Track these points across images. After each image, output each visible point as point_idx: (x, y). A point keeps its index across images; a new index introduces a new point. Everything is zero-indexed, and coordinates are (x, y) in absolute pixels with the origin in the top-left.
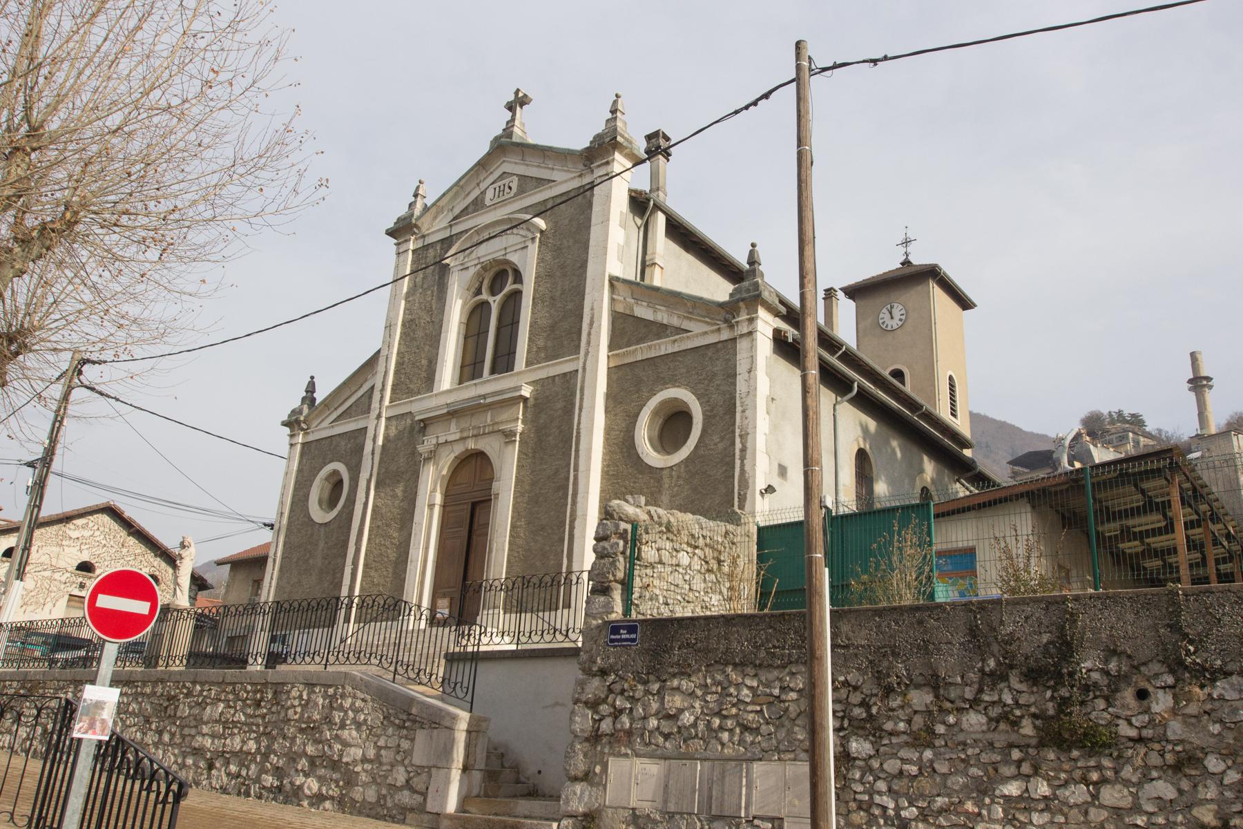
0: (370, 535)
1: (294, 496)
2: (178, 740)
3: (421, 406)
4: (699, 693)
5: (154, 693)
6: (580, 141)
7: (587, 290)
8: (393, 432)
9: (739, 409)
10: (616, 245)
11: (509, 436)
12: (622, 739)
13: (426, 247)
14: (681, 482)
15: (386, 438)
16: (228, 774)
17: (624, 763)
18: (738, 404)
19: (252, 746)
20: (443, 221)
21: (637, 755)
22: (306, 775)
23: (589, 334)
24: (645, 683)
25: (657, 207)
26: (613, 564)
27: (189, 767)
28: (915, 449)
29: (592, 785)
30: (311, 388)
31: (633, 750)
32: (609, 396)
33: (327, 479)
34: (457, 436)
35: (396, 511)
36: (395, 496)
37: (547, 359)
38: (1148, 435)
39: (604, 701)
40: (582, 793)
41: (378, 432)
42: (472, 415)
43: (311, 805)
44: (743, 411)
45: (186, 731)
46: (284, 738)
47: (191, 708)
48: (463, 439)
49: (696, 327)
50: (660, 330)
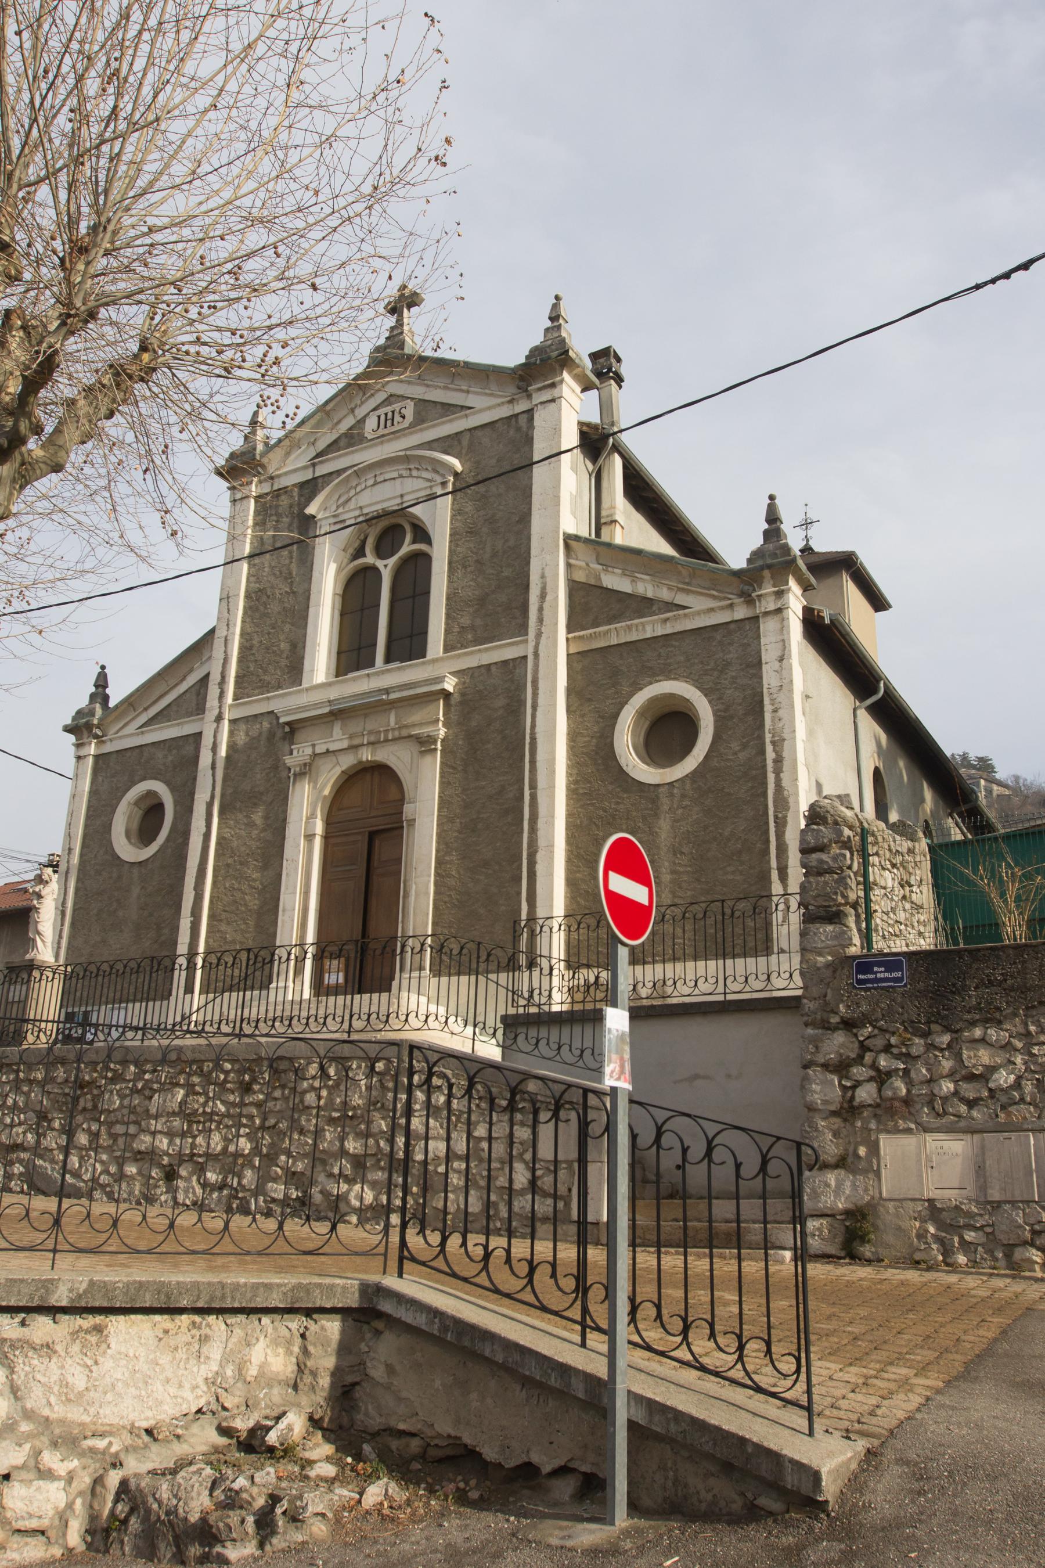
0: (215, 876)
1: (86, 826)
2: (104, 1140)
3: (286, 703)
4: (1019, 1044)
5: (49, 1079)
6: (514, 357)
7: (533, 552)
8: (241, 738)
9: (768, 708)
10: (567, 498)
11: (425, 744)
12: (892, 1112)
13: (277, 494)
14: (686, 802)
15: (232, 747)
16: (205, 1185)
17: (908, 1143)
18: (767, 701)
19: (245, 1145)
20: (300, 458)
21: (926, 1130)
22: (350, 1181)
23: (541, 609)
24: (925, 1035)
25: (617, 448)
26: (842, 881)
27: (132, 1178)
28: (917, 773)
29: (854, 1171)
30: (102, 682)
31: (917, 1123)
32: (569, 691)
33: (137, 803)
34: (345, 744)
35: (254, 844)
36: (252, 825)
37: (478, 641)
38: (999, 783)
39: (859, 1060)
40: (839, 1185)
41: (218, 739)
42: (366, 716)
43: (360, 1222)
44: (775, 711)
45: (119, 1129)
46: (302, 1132)
47: (122, 1097)
48: (353, 748)
49: (696, 602)
50: (644, 606)
